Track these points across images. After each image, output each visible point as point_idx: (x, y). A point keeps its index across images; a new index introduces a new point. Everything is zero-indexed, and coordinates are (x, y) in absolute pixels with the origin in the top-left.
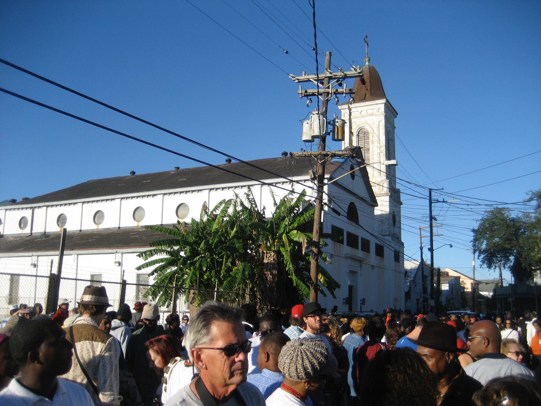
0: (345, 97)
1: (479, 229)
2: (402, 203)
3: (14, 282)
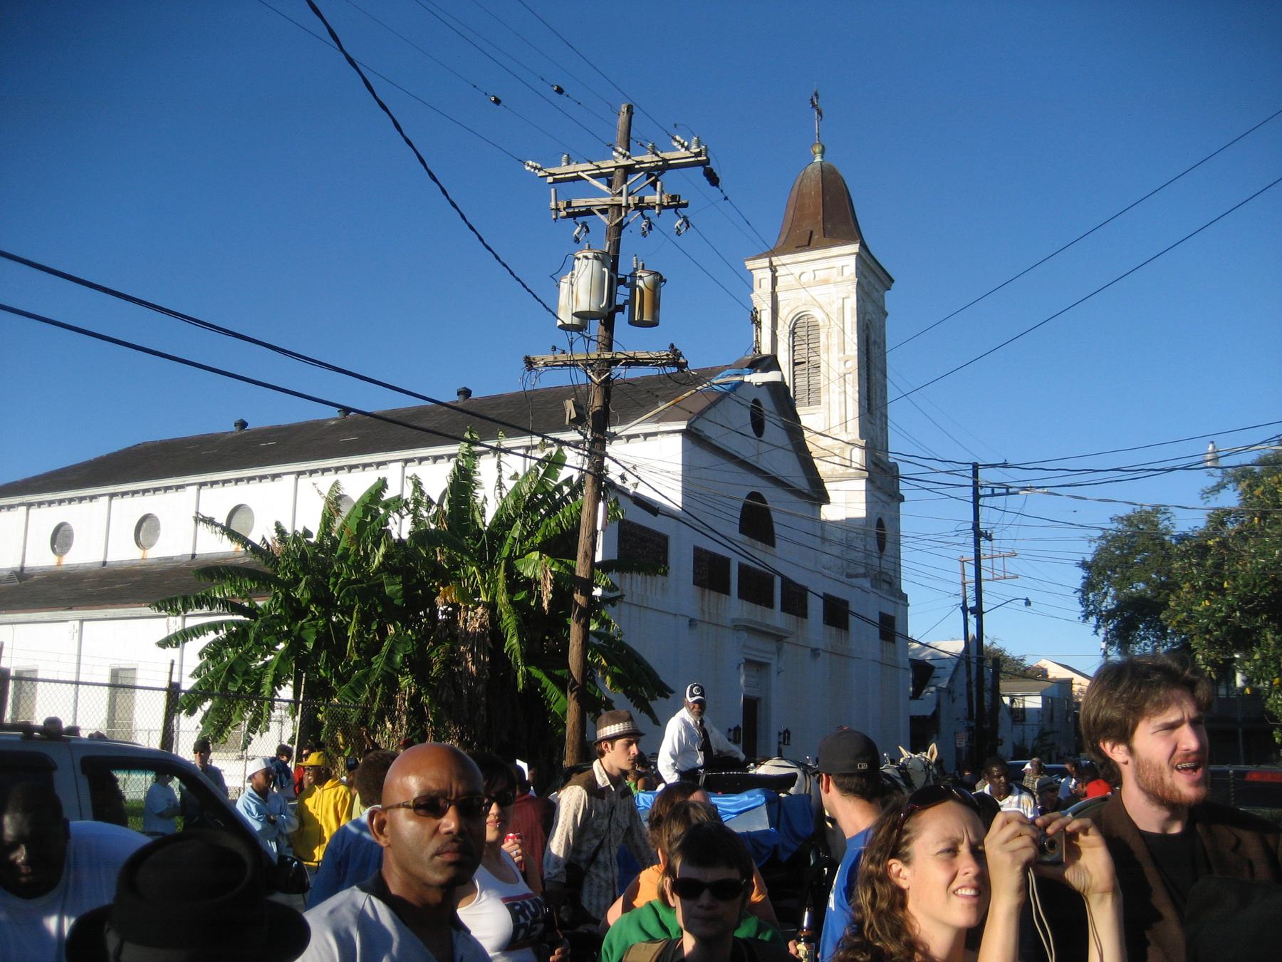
0: (659, 214)
1: (1093, 561)
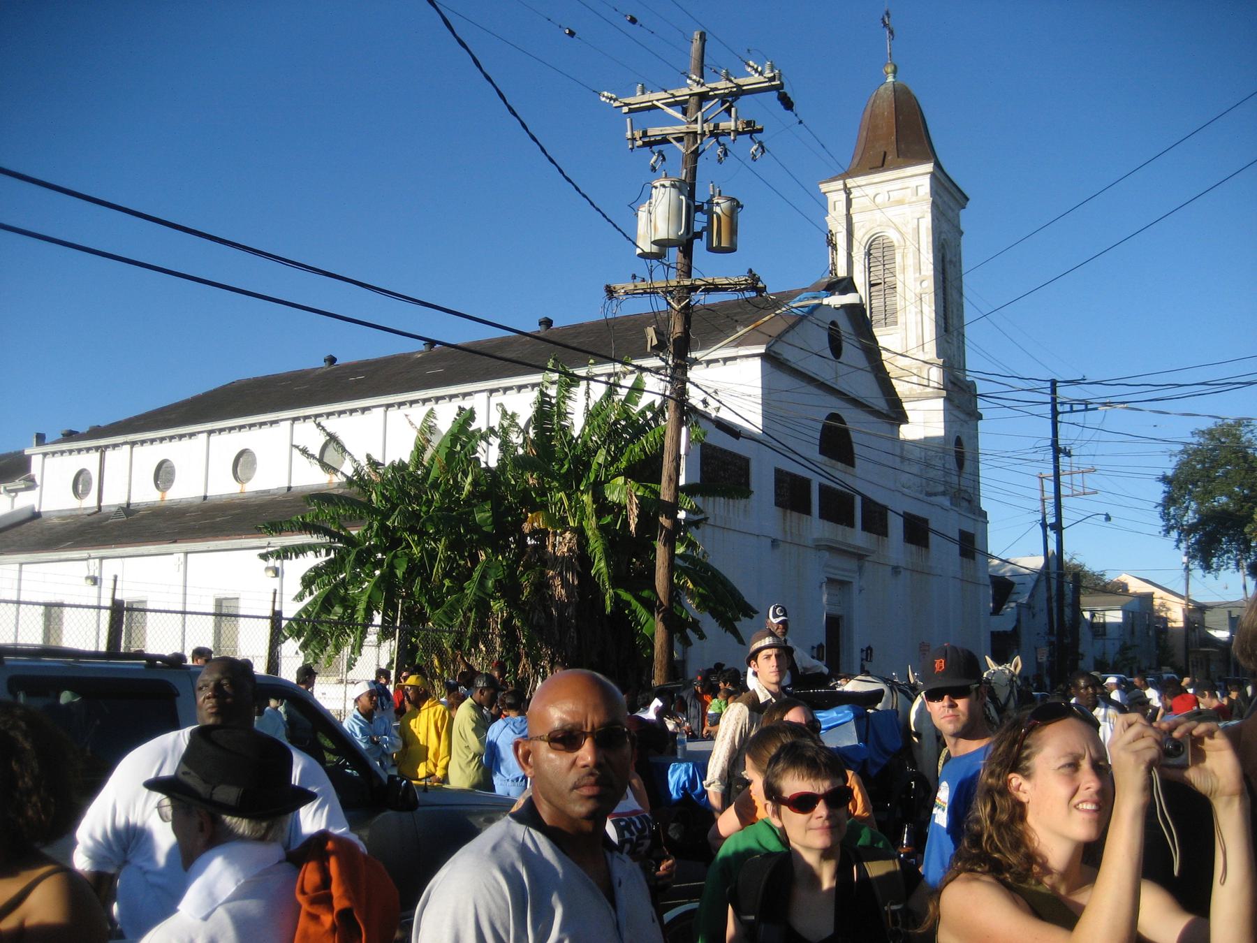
0: (734, 140)
1: (1175, 475)
2: (981, 415)
3: (52, 619)
